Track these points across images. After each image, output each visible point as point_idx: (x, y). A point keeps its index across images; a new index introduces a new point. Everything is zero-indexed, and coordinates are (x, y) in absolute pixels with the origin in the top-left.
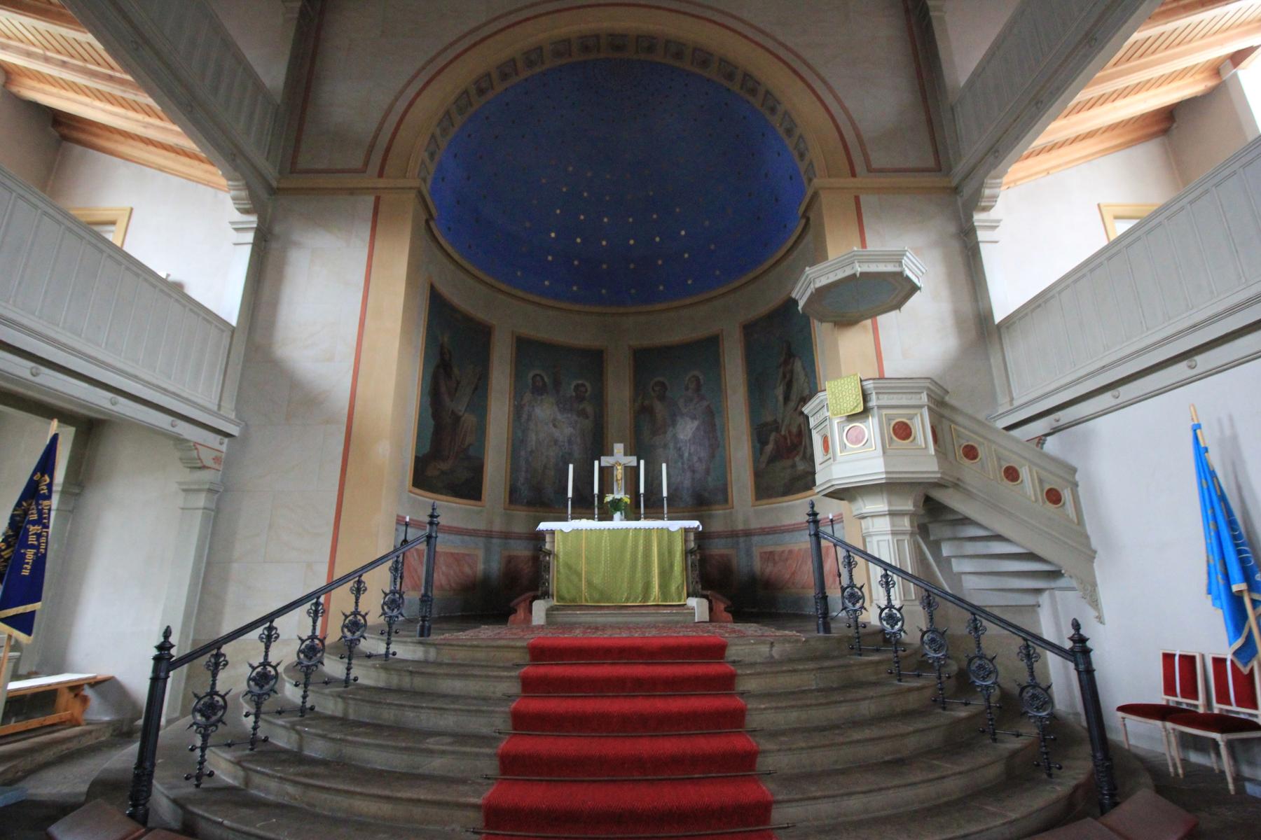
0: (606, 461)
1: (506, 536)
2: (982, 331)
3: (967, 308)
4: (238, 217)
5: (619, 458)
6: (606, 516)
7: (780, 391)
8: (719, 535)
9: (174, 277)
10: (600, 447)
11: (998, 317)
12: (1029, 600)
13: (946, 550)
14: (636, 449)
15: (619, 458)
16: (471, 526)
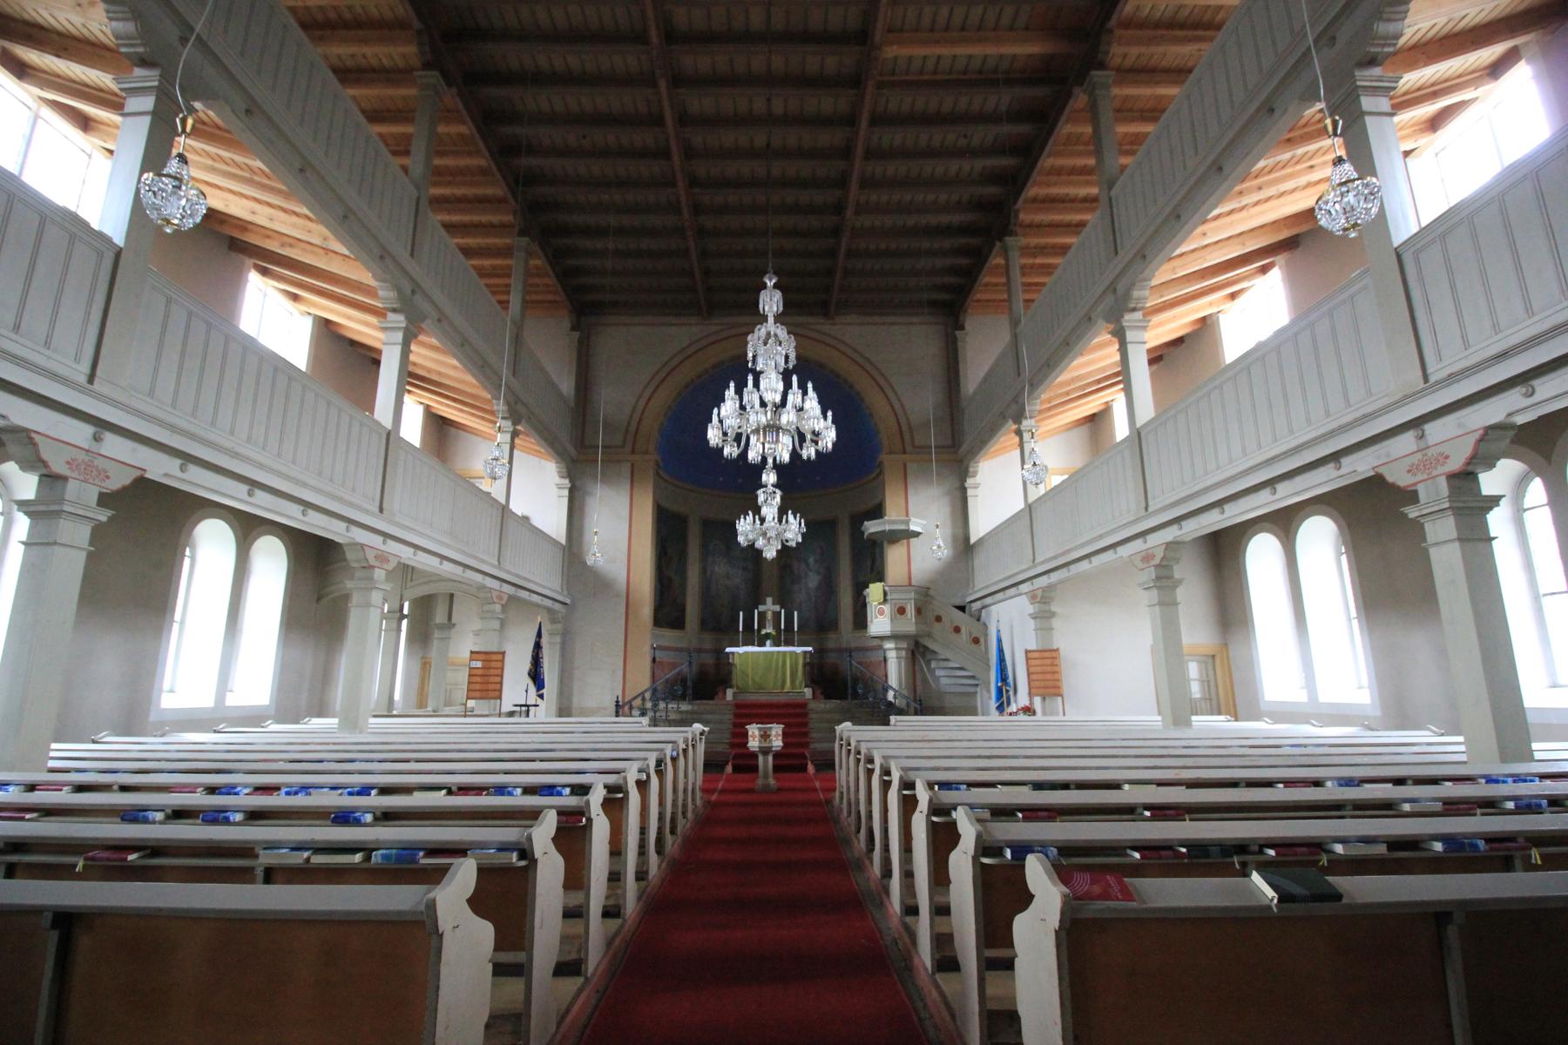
0: (761, 608)
1: (699, 651)
2: (965, 548)
3: (960, 532)
4: (558, 480)
5: (770, 606)
6: (762, 644)
7: (869, 563)
8: (832, 650)
9: (526, 513)
10: (759, 601)
11: (973, 541)
12: (971, 690)
13: (933, 665)
14: (782, 601)
15: (770, 606)
16: (680, 645)
